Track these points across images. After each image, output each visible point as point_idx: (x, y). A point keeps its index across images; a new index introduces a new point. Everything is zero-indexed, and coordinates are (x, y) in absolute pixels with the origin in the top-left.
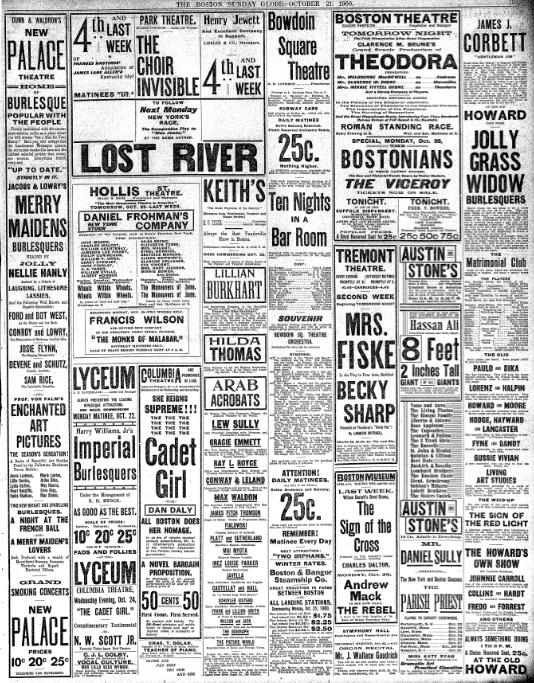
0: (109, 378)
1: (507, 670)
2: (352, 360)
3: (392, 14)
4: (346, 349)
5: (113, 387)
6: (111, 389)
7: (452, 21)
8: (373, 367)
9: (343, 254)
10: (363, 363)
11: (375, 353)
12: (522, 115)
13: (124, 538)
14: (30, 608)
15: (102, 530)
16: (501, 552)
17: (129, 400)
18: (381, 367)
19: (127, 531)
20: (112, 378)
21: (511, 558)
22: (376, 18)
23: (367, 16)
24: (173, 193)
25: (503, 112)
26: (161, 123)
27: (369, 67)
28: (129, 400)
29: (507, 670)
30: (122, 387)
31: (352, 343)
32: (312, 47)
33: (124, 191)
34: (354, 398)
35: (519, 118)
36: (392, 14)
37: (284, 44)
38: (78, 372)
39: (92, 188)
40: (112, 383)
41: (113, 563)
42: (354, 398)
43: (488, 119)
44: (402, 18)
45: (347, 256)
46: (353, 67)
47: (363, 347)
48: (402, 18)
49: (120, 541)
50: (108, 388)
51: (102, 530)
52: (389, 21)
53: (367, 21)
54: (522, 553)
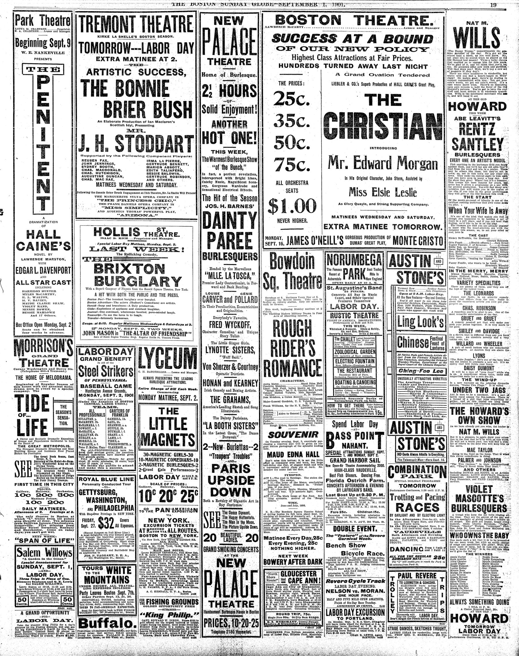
0: (172, 358)
1: (229, 468)
5: (176, 367)
6: (174, 369)
12: (502, 106)
13: (186, 498)
15: (166, 490)
17: (191, 379)
19: (190, 491)
20: (175, 359)
23: (313, 17)
24: (171, 234)
27: (393, 104)
28: (191, 379)
29: (229, 468)
30: (185, 368)
34: (242, 248)
37: (269, 280)
38: (143, 351)
39: (95, 229)
40: (175, 363)
42: (242, 248)
44: (363, 20)
48: (363, 20)
49: (183, 501)
50: (171, 368)
51: (166, 490)
54: (503, 411)
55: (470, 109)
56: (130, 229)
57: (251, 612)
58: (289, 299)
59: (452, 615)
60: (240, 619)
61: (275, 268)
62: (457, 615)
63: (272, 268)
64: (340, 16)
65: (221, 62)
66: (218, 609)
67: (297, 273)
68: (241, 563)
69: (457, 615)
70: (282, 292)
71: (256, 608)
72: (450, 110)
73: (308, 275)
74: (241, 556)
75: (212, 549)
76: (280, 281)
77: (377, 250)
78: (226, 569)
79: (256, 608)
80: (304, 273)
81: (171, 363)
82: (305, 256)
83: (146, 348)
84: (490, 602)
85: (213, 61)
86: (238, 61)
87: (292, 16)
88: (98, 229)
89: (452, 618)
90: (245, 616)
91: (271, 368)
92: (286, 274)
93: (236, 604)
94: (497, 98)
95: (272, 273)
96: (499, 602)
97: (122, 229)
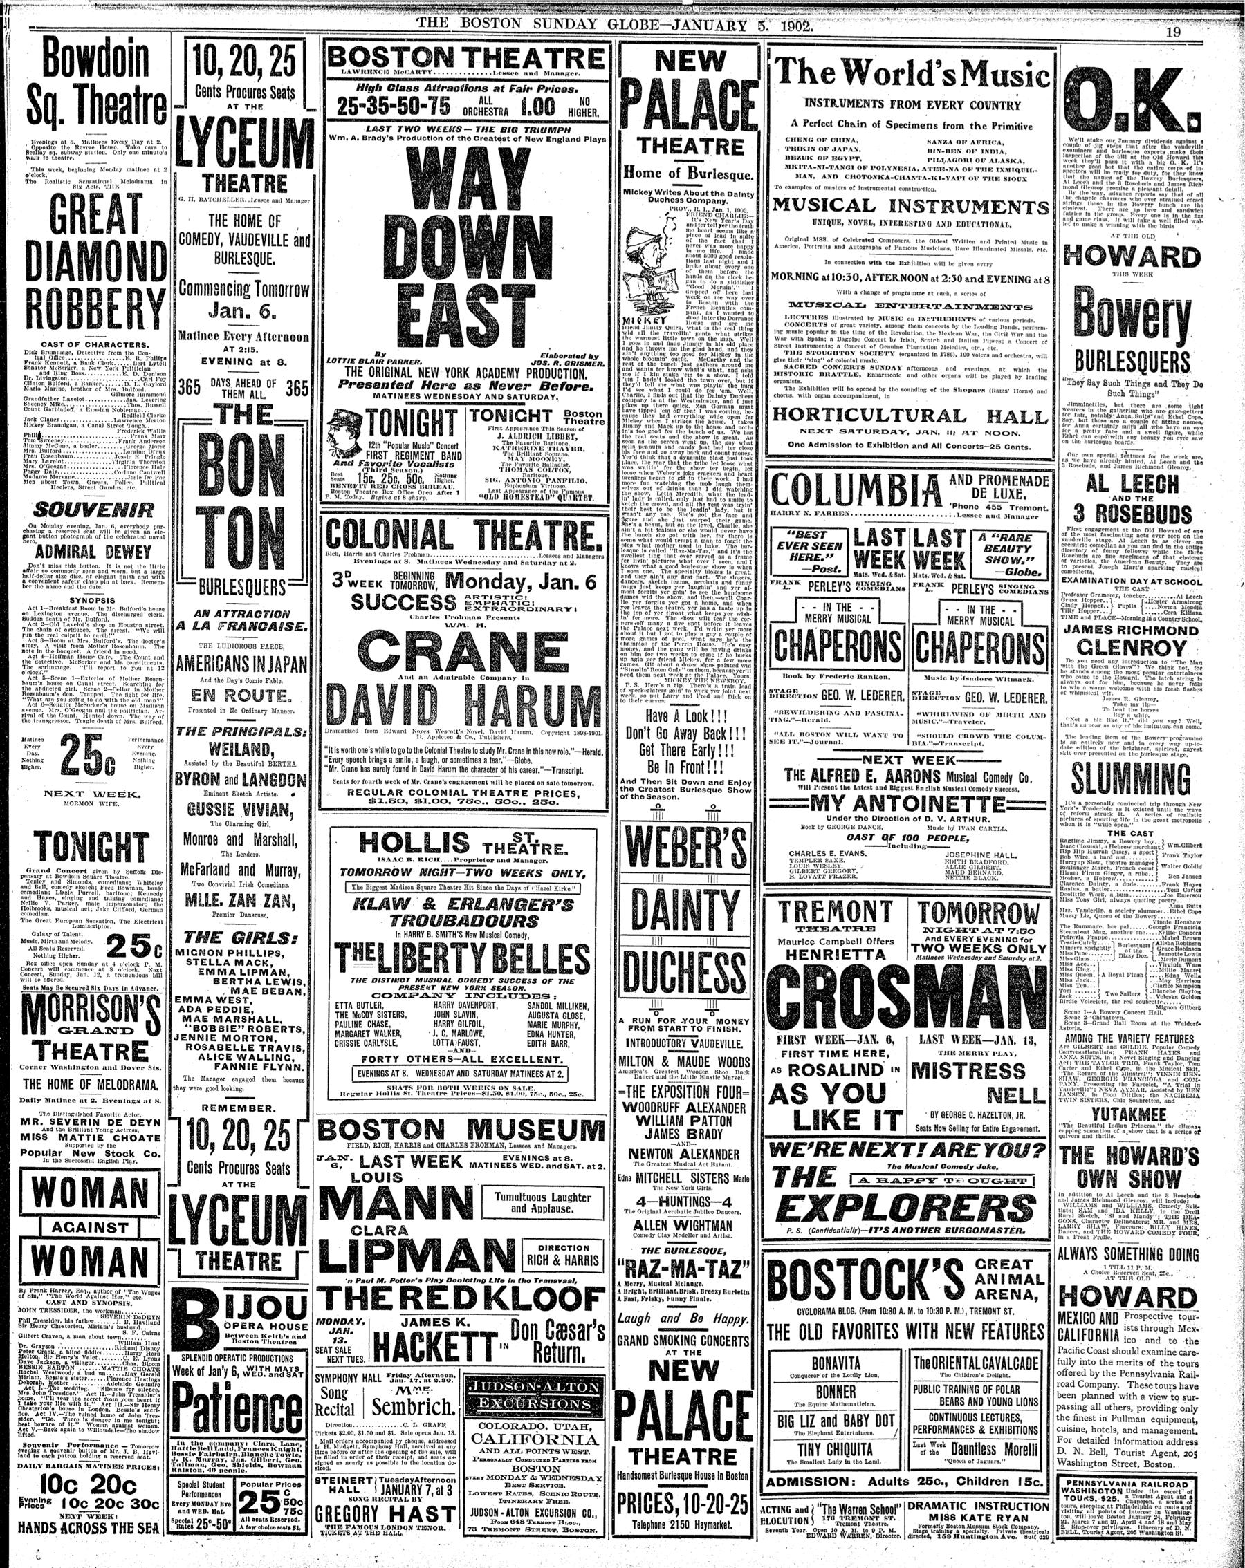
3: (458, 47)
9: (559, 530)
16: (1138, 1156)
21: (1163, 1168)
23: (400, 51)
25: (1145, 1290)
26: (220, 258)
27: (507, 66)
32: (156, 108)
33: (437, 842)
35: (1186, 264)
36: (458, 47)
37: (40, 101)
39: (363, 835)
41: (256, 1198)
43: (1116, 263)
45: (566, 536)
46: (487, 65)
54: (1186, 1156)
56: (446, 835)
57: (729, 1476)
58: (86, 147)
60: (703, 1493)
61: (55, 74)
63: (47, 73)
65: (672, 146)
66: (652, 1467)
67: (108, 85)
68: (708, 1370)
70: (71, 131)
71: (742, 1465)
72: (1067, 262)
73: (132, 92)
74: (710, 1354)
75: (641, 1341)
76: (67, 106)
77: (816, 462)
78: (671, 1384)
79: (742, 1465)
80: (125, 85)
82: (126, 45)
85: (650, 144)
86: (713, 146)
88: (369, 837)
90: (715, 1486)
91: (43, 308)
92: (81, 87)
93: (693, 1457)
95: (48, 85)
97: (427, 835)
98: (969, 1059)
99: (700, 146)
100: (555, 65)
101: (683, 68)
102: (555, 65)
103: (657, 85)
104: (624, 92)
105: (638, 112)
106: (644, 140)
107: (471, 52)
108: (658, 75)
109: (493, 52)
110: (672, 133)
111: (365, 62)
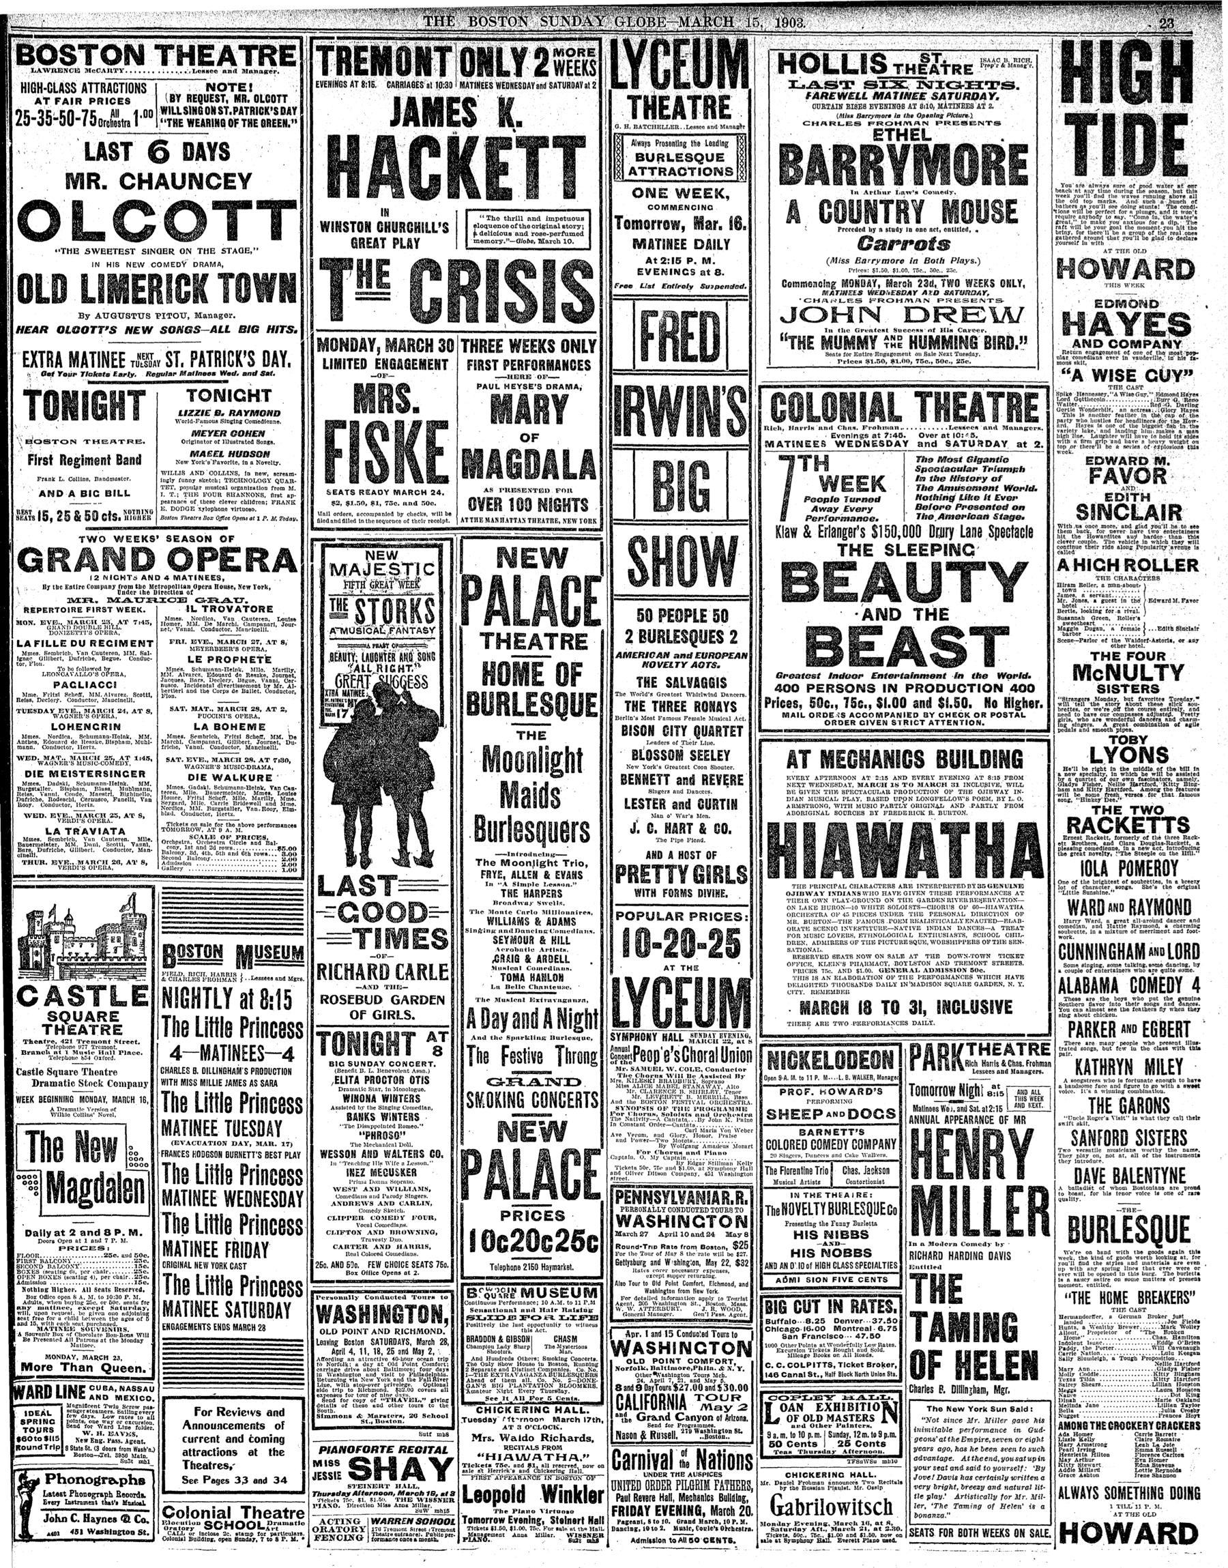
2: (354, 461)
3: (149, 45)
4: (342, 439)
7: (283, 63)
8: (400, 479)
9: (700, 103)
10: (377, 470)
11: (405, 450)
14: (69, 175)
18: (417, 478)
22: (111, 55)
23: (89, 49)
31: (355, 424)
36: (149, 45)
38: (623, 986)
40: (703, 348)
46: (180, 63)
47: (377, 434)
50: (689, 1025)
52: (140, 60)
53: (89, 62)
55: (1109, 276)
56: (864, 57)
59: (1063, 1525)
62: (1075, 1525)
64: (141, 47)
69: (1075, 1525)
81: (688, 1013)
83: (629, 981)
84: (1155, 1493)
85: (493, 640)
86: (557, 641)
87: (47, 46)
88: (787, 58)
89: (1064, 1532)
94: (1171, 250)
96: (1177, 1493)
97: (845, 57)
98: (419, 1303)
99: (545, 642)
100: (249, 62)
101: (525, 565)
102: (249, 62)
103: (497, 582)
104: (465, 589)
105: (478, 609)
106: (487, 635)
107: (164, 49)
108: (498, 572)
109: (186, 49)
110: (513, 629)
111: (52, 61)
